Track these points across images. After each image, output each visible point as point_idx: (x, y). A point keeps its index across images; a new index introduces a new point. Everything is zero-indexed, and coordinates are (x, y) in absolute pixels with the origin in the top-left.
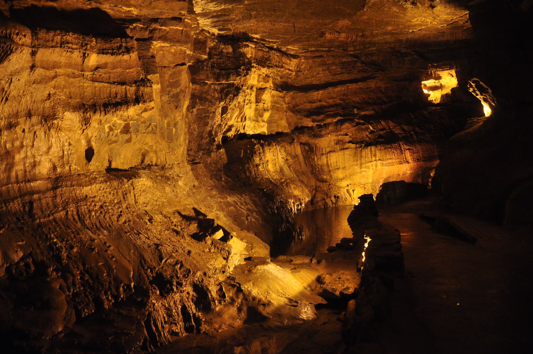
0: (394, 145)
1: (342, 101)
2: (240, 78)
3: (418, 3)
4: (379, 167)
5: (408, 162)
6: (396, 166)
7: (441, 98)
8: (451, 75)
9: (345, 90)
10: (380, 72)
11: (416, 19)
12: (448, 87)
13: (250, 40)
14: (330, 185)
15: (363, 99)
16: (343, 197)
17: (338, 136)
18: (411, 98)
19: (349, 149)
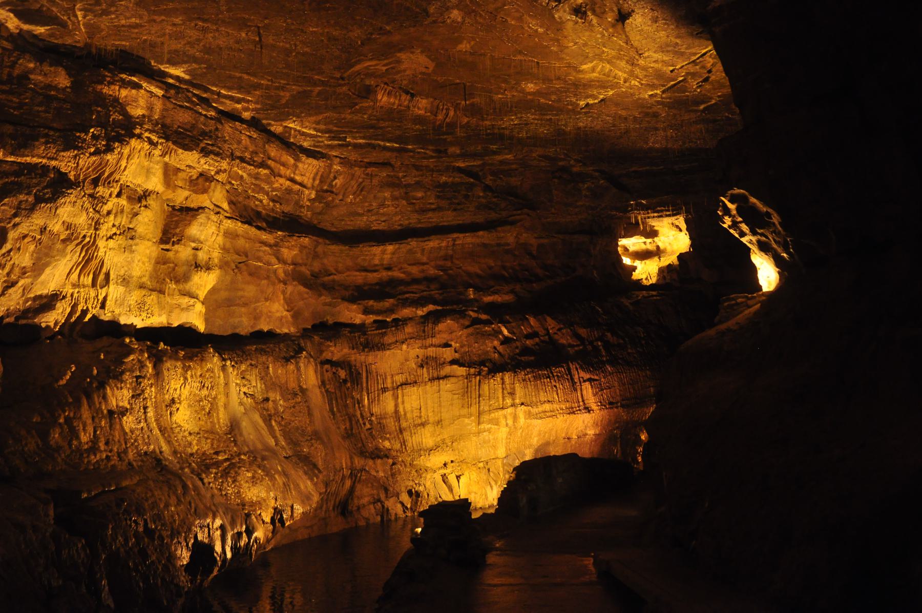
0: (556, 371)
1: (441, 270)
2: (75, 157)
3: (589, 13)
4: (522, 420)
5: (588, 410)
6: (561, 418)
7: (658, 275)
8: (677, 227)
9: (447, 246)
10: (526, 210)
11: (590, 65)
12: (673, 253)
13: (157, 77)
14: (394, 464)
15: (490, 268)
16: (432, 493)
17: (426, 348)
18: (595, 272)
19: (453, 380)
